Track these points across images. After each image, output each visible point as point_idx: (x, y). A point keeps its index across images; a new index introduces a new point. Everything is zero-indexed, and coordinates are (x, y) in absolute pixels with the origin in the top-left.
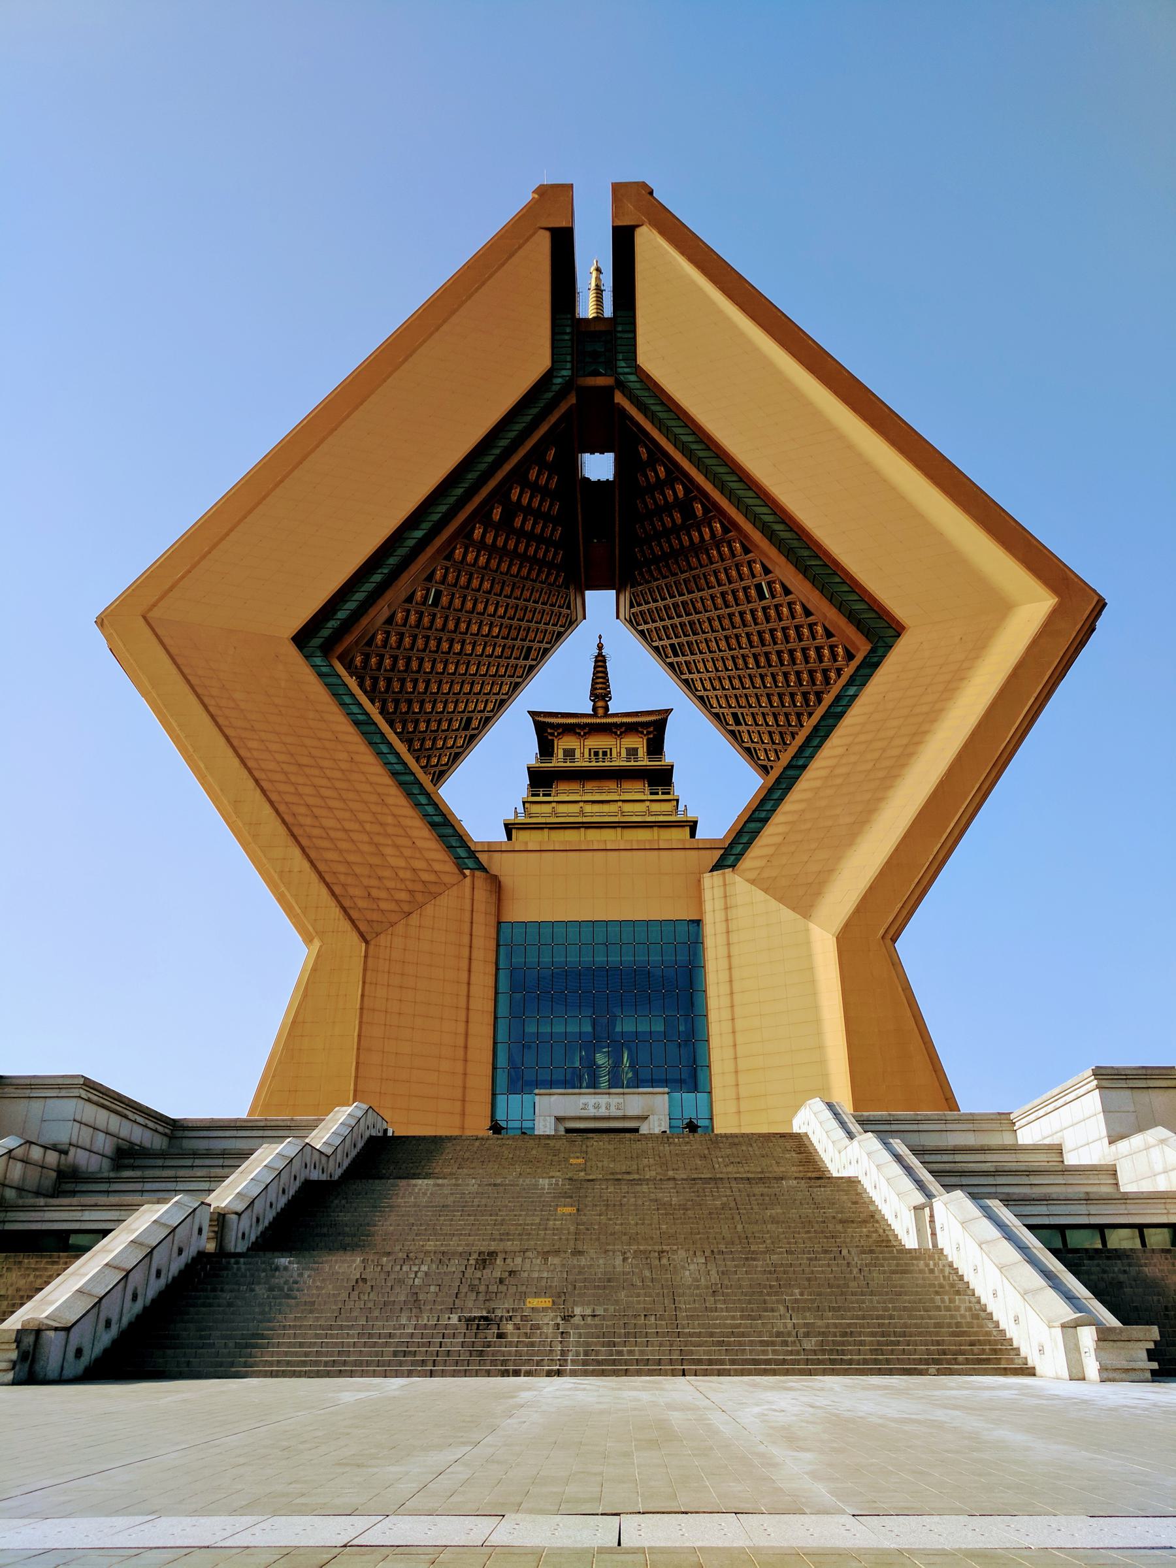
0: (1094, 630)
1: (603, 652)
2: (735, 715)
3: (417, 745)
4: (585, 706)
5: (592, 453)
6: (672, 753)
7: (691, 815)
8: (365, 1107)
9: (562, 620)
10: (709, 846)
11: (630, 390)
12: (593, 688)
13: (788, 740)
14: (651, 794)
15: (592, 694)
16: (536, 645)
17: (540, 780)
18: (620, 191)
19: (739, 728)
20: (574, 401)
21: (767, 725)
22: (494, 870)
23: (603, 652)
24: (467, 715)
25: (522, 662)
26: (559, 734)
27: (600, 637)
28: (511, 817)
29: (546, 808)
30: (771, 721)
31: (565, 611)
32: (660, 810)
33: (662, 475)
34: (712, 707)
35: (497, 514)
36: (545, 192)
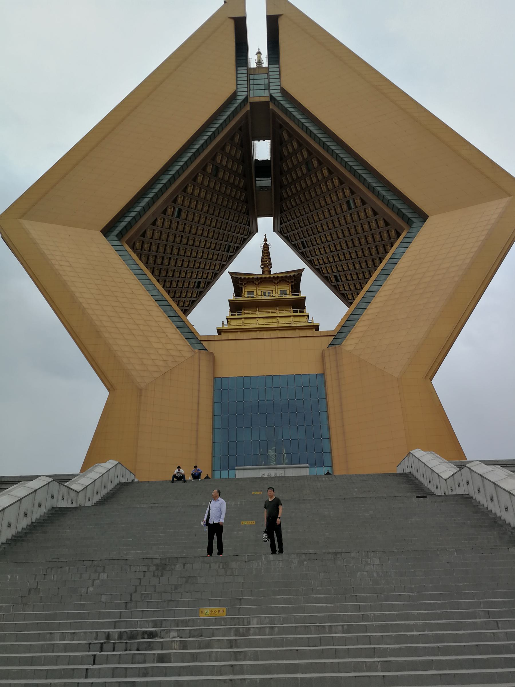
1: (266, 246)
2: (336, 277)
3: (168, 285)
4: (257, 270)
5: (259, 141)
7: (316, 322)
8: (116, 462)
9: (246, 232)
10: (327, 335)
11: (278, 101)
12: (262, 261)
14: (294, 312)
15: (262, 265)
16: (232, 245)
17: (236, 307)
20: (249, 109)
22: (211, 350)
23: (266, 246)
24: (197, 280)
26: (245, 284)
27: (265, 235)
28: (220, 326)
30: (355, 277)
32: (299, 322)
34: (324, 274)
35: (209, 169)
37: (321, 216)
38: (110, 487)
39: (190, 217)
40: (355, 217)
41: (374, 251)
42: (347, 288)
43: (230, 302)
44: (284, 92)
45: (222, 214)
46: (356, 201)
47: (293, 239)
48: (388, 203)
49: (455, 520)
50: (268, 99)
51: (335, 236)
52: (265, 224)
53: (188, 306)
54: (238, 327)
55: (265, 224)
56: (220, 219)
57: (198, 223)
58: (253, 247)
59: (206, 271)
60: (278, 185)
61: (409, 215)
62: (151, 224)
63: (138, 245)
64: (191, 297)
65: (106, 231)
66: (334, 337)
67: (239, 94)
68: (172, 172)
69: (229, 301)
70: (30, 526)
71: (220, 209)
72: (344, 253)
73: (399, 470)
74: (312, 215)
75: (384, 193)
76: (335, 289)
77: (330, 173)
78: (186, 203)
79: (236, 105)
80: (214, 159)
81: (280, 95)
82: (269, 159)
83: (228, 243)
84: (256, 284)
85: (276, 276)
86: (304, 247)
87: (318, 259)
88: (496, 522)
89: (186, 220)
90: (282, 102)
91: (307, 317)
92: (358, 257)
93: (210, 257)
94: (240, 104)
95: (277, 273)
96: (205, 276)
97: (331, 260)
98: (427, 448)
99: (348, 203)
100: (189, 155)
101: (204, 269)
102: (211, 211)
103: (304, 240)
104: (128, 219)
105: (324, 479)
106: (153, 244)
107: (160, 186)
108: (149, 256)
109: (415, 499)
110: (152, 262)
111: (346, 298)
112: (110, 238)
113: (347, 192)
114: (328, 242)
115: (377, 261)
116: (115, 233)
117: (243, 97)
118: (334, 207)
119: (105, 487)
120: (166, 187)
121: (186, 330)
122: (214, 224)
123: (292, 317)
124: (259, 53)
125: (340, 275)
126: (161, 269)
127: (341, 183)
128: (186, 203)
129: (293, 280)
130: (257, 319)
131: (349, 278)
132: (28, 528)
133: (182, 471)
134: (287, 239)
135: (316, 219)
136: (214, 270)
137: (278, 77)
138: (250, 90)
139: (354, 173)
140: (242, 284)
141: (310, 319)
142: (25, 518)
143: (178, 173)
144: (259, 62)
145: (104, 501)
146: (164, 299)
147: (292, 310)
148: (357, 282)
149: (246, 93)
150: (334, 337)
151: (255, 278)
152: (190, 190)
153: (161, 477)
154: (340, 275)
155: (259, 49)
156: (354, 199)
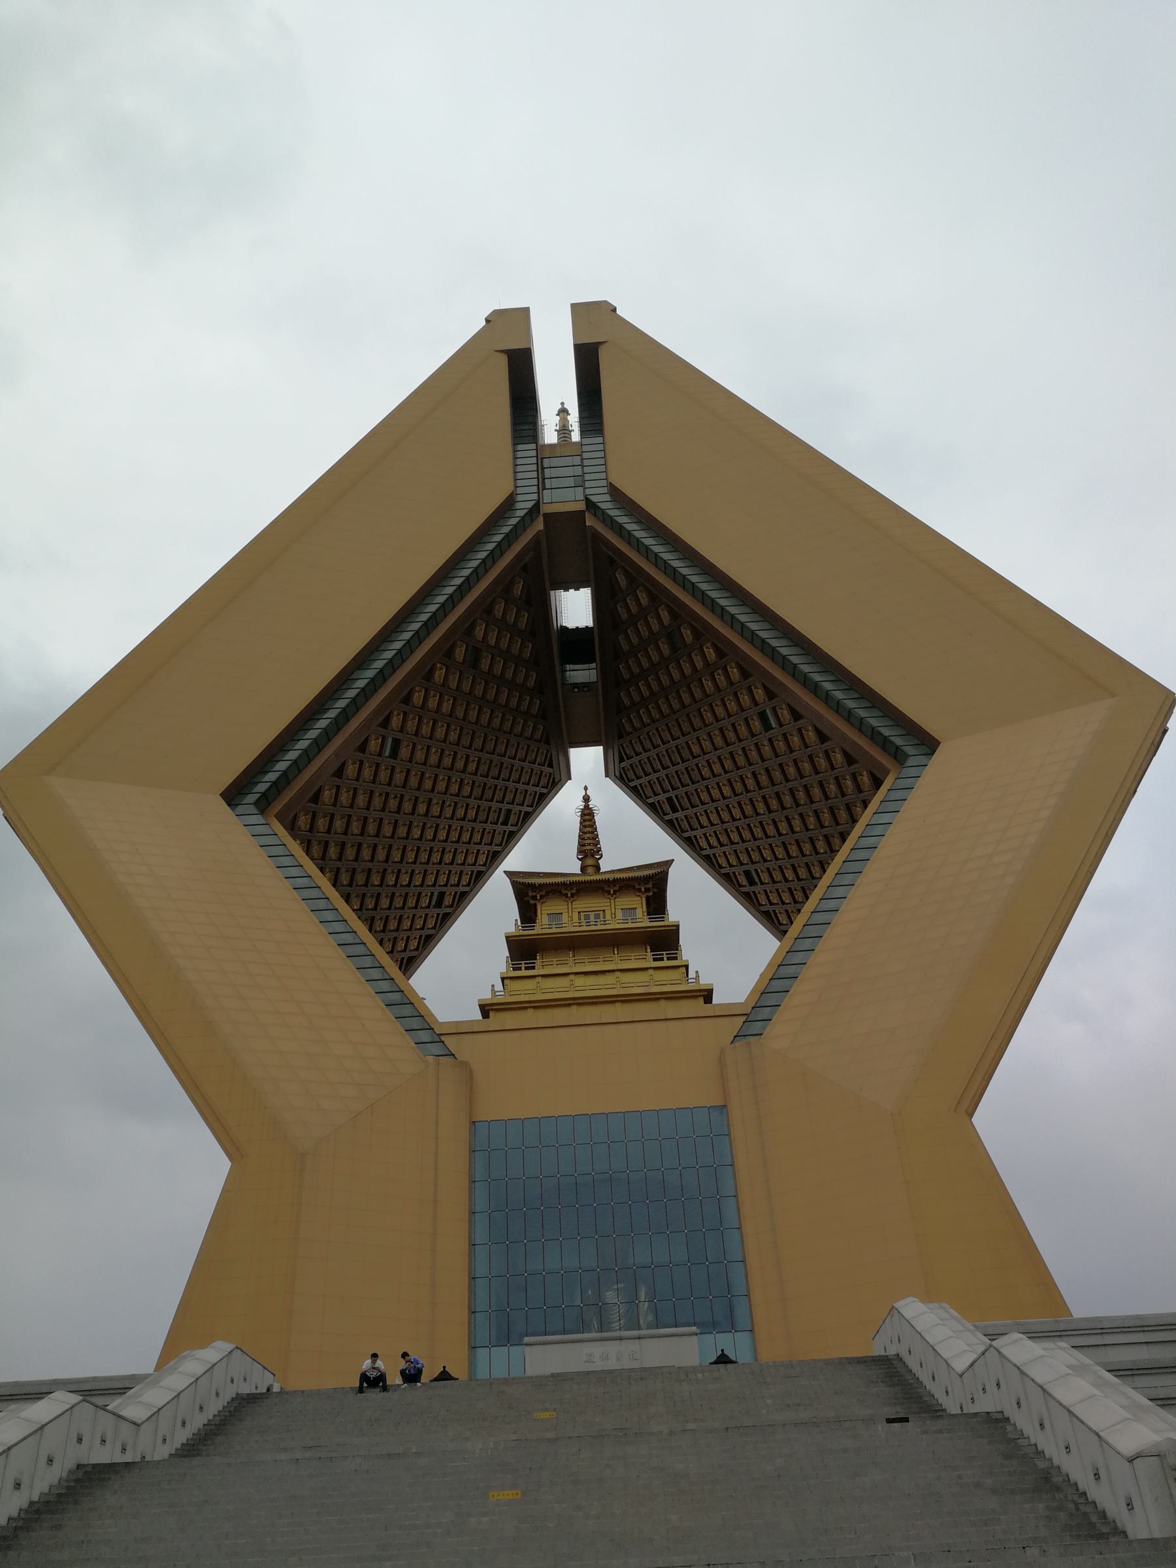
0: (1166, 731)
1: (589, 812)
2: (747, 873)
4: (570, 865)
5: (566, 590)
6: (675, 911)
7: (704, 981)
8: (229, 1347)
9: (544, 781)
10: (728, 1013)
11: (603, 512)
12: (581, 845)
13: (816, 871)
14: (655, 960)
15: (580, 852)
17: (523, 950)
18: (579, 310)
19: (753, 888)
21: (786, 880)
23: (589, 812)
25: (500, 828)
26: (542, 897)
27: (586, 788)
28: (487, 996)
29: (530, 984)
30: (790, 875)
31: (546, 769)
32: (666, 981)
33: (644, 601)
34: (721, 867)
35: (460, 653)
36: (496, 319)
37: (707, 745)
38: (215, 1407)
39: (420, 755)
40: (781, 746)
41: (826, 817)
42: (774, 898)
43: (511, 941)
44: (615, 493)
45: (490, 746)
46: (779, 711)
47: (649, 792)
48: (849, 716)
49: (960, 1477)
50: (582, 506)
51: (738, 787)
52: (587, 760)
53: (417, 949)
54: (526, 998)
55: (587, 760)
56: (485, 757)
57: (438, 767)
58: (563, 806)
59: (456, 869)
60: (611, 680)
61: (898, 741)
62: (334, 775)
63: (303, 821)
64: (422, 928)
65: (233, 795)
66: (744, 1018)
67: (519, 498)
68: (379, 664)
69: (507, 938)
70: (26, 1511)
71: (486, 735)
72: (761, 823)
73: (877, 1350)
74: (687, 743)
75: (839, 695)
76: (749, 900)
77: (721, 654)
78: (411, 726)
79: (514, 521)
80: (470, 631)
81: (608, 498)
82: (590, 624)
83: (505, 807)
84: (566, 895)
85: (611, 877)
86: (675, 810)
87: (705, 835)
88: (1047, 1479)
89: (410, 761)
90: (612, 513)
91: (684, 970)
92: (793, 832)
93: (466, 837)
94: (523, 518)
95: (613, 871)
96: (454, 879)
97: (735, 837)
98: (928, 1296)
99: (763, 716)
100: (415, 626)
101: (452, 863)
102: (466, 741)
103: (672, 794)
104: (282, 766)
105: (700, 1375)
106: (337, 817)
107: (352, 693)
108: (327, 843)
109: (882, 1428)
110: (334, 857)
111: (775, 921)
112: (240, 809)
113: (760, 694)
114: (724, 798)
115: (836, 841)
116: (251, 798)
117: (530, 505)
118: (733, 725)
119: (201, 1408)
120: (365, 695)
121: (407, 1010)
122: (472, 767)
123: (651, 972)
124: (563, 412)
125: (756, 870)
126: (354, 869)
127: (745, 674)
128: (411, 726)
129: (650, 886)
130: (572, 977)
131: (777, 876)
132: (22, 1515)
133: (379, 1363)
134: (637, 793)
135: (696, 749)
136: (474, 864)
137: (602, 461)
138: (544, 489)
139: (773, 654)
140: (534, 898)
141: (692, 974)
142: (17, 1493)
143: (392, 666)
144: (564, 431)
145: (190, 1450)
146: (357, 941)
147: (649, 955)
148: (795, 885)
149: (535, 497)
150: (744, 1018)
151: (564, 884)
152: (418, 698)
153: (330, 1383)
154: (756, 870)
155: (562, 404)
156: (774, 709)
